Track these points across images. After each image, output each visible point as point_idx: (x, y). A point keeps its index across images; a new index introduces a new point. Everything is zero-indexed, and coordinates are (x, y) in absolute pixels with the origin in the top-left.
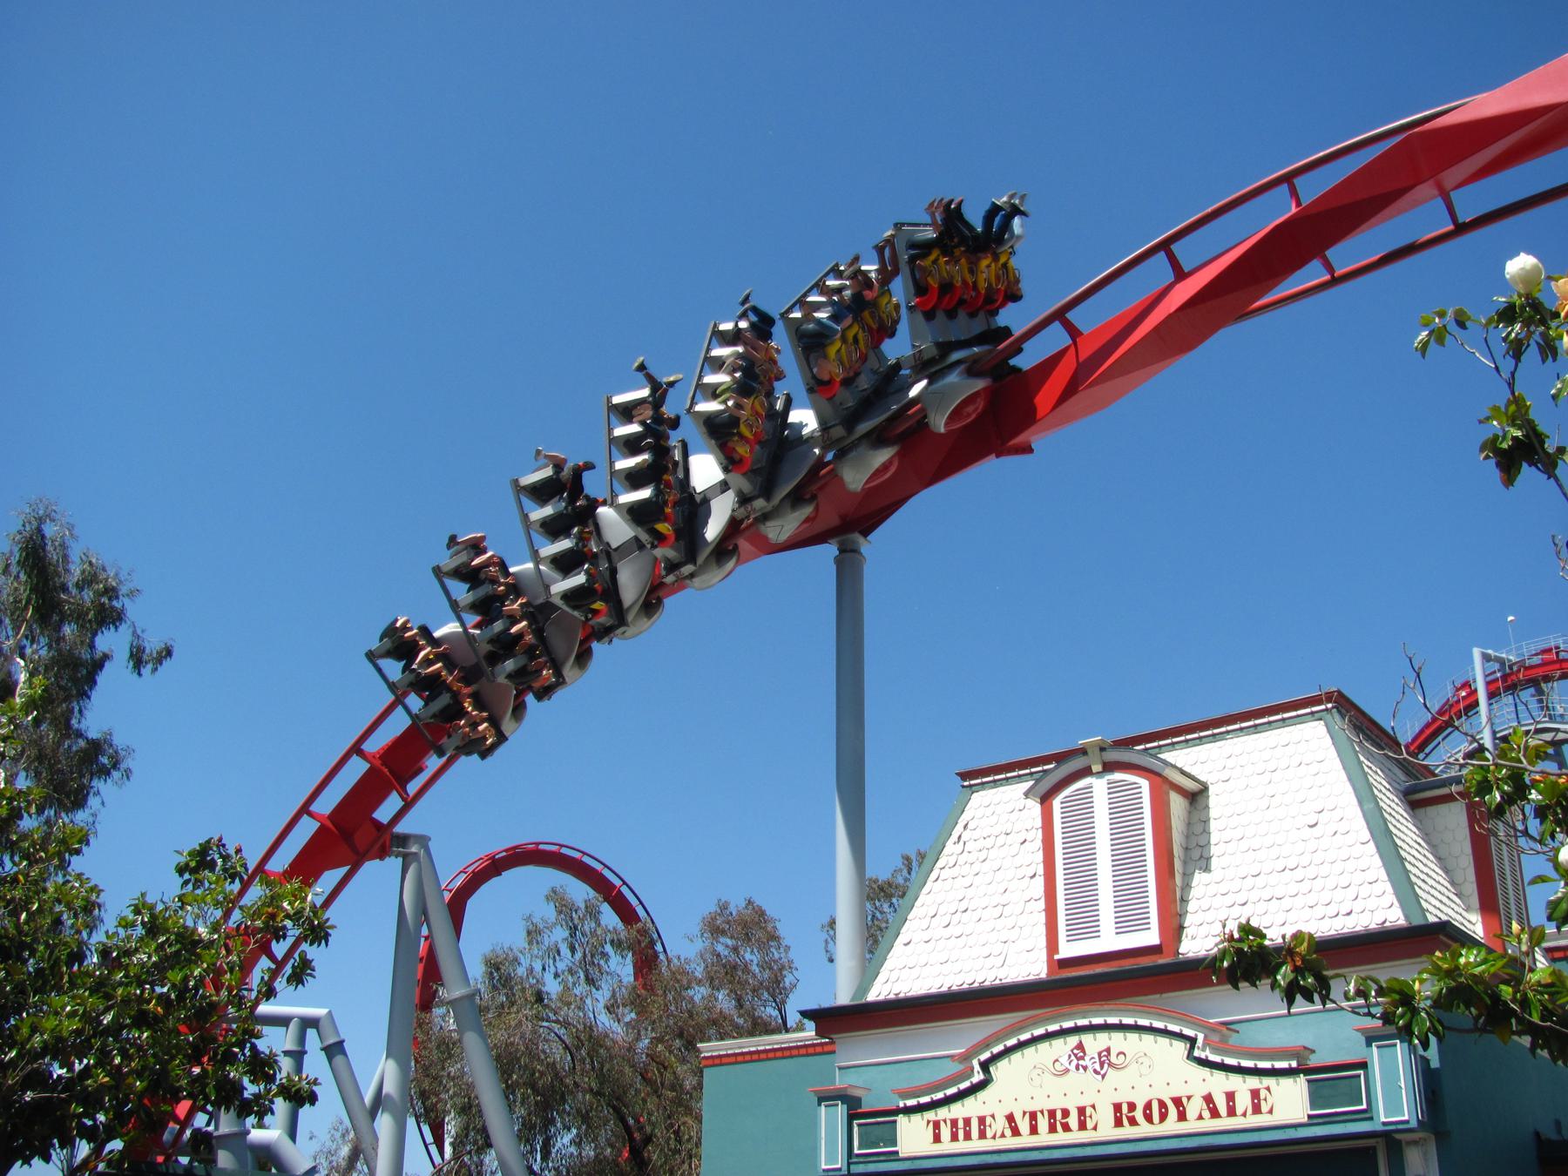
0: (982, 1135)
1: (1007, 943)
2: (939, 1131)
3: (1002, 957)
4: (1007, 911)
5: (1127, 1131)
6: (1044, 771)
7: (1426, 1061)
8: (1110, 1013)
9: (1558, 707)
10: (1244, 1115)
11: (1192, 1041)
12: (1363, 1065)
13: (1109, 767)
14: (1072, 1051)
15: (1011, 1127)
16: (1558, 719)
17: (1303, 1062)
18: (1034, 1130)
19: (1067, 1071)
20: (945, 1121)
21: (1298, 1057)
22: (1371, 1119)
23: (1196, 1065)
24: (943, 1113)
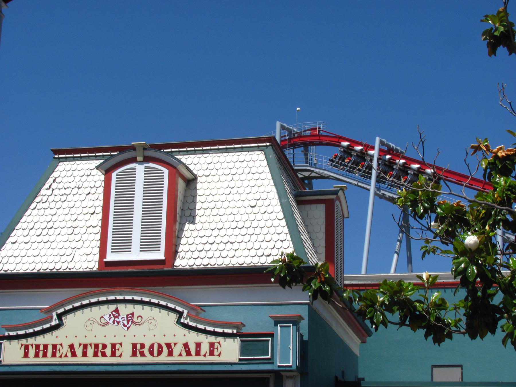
0: (54, 355)
1: (75, 250)
2: (87, 350)
3: (72, 256)
4: (76, 231)
5: (139, 359)
6: (111, 155)
7: (301, 336)
8: (136, 294)
9: (314, 159)
10: (205, 356)
11: (181, 314)
12: (272, 335)
13: (147, 159)
14: (112, 313)
15: (71, 352)
16: (313, 166)
17: (239, 331)
18: (85, 354)
19: (108, 323)
20: (32, 345)
21: (237, 328)
22: (273, 363)
23: (181, 327)
24: (31, 341)
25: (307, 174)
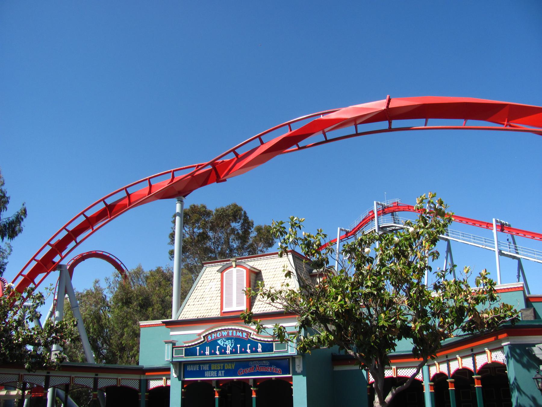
25: (394, 228)
